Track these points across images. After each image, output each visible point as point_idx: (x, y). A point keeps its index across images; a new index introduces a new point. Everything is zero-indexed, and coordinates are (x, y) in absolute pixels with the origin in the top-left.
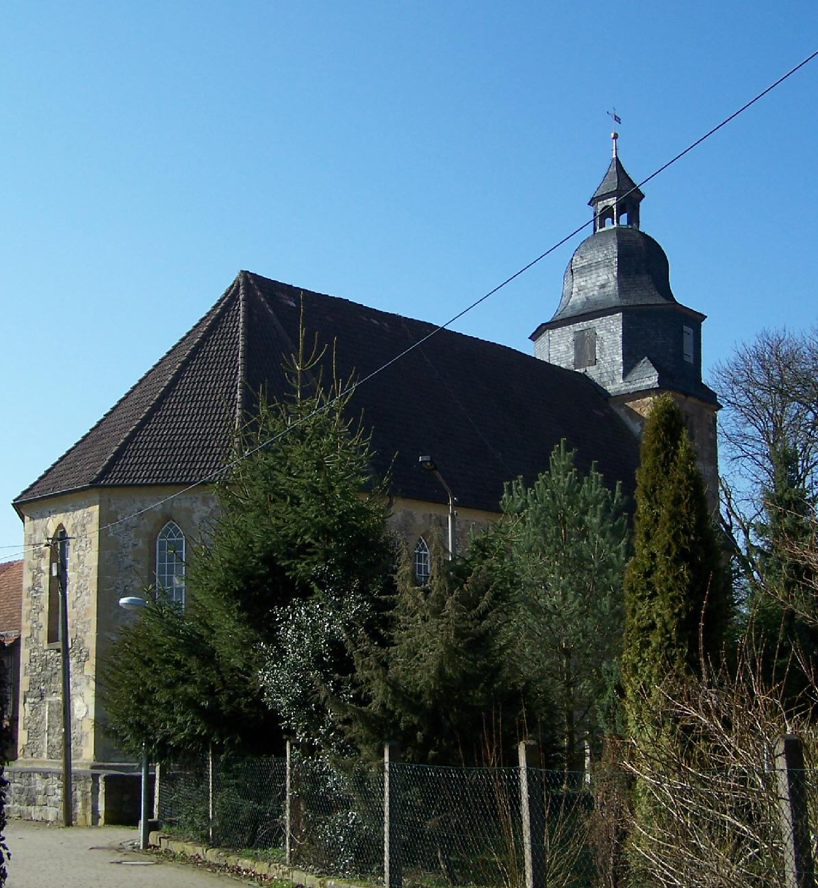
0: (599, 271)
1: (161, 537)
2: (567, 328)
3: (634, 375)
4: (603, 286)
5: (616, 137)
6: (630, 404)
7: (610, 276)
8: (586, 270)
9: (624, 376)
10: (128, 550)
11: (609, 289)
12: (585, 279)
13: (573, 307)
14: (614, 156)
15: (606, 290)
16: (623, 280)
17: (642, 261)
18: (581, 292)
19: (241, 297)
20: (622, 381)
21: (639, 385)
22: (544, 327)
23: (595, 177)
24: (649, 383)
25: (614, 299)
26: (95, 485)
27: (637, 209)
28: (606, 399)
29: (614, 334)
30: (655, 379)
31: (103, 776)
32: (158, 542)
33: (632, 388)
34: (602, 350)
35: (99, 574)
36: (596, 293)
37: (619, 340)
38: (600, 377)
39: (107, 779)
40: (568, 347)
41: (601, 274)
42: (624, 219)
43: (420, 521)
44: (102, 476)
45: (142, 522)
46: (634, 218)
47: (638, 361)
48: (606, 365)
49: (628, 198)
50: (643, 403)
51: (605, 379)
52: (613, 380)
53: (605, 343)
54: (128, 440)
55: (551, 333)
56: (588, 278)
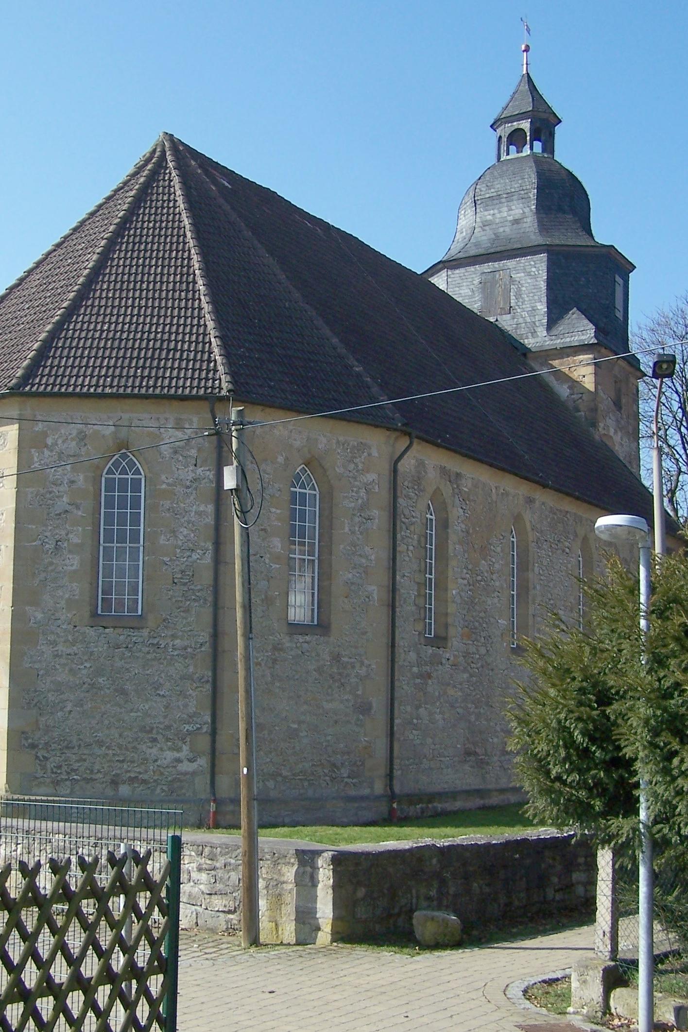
0: (510, 204)
1: (110, 472)
2: (472, 269)
3: (561, 328)
4: (516, 222)
5: (527, 50)
6: (556, 363)
7: (527, 210)
8: (496, 202)
9: (550, 327)
10: (61, 489)
11: (525, 225)
12: (492, 212)
13: (477, 245)
14: (525, 72)
15: (520, 226)
16: (544, 216)
17: (562, 198)
18: (487, 228)
19: (171, 165)
20: (545, 333)
21: (568, 340)
22: (441, 266)
23: (499, 94)
24: (583, 337)
25: (533, 237)
26: (16, 392)
27: (552, 135)
28: (525, 355)
29: (535, 277)
30: (592, 333)
31: (328, 855)
32: (103, 479)
33: (558, 343)
34: (518, 295)
35: (17, 522)
36: (507, 229)
37: (543, 285)
38: (516, 329)
39: (339, 860)
40: (473, 291)
41: (513, 207)
42: (538, 146)
43: (432, 475)
44: (18, 386)
45: (83, 449)
46: (549, 148)
47: (567, 311)
48: (525, 314)
49: (544, 125)
50: (574, 362)
51: (523, 331)
52: (534, 333)
53: (524, 289)
54: (53, 335)
55: (449, 273)
56: (496, 211)
